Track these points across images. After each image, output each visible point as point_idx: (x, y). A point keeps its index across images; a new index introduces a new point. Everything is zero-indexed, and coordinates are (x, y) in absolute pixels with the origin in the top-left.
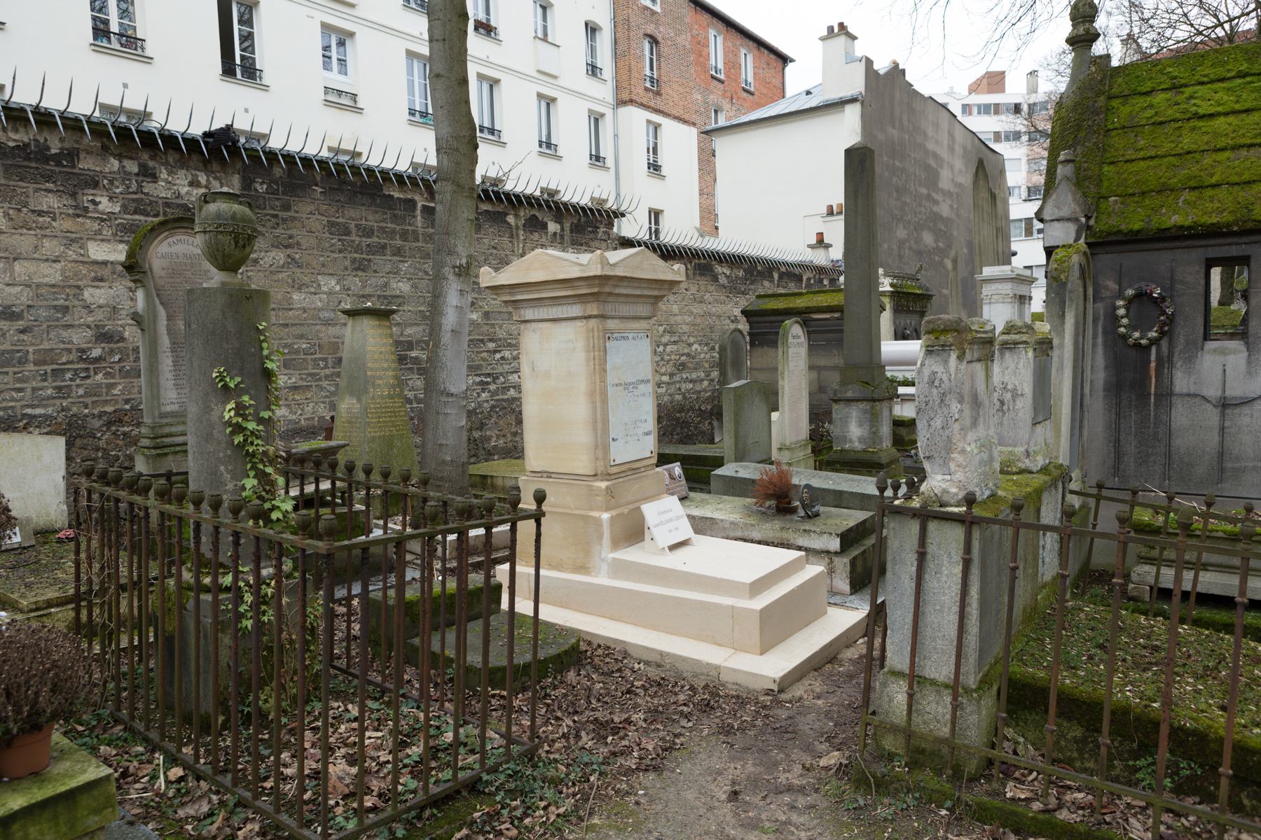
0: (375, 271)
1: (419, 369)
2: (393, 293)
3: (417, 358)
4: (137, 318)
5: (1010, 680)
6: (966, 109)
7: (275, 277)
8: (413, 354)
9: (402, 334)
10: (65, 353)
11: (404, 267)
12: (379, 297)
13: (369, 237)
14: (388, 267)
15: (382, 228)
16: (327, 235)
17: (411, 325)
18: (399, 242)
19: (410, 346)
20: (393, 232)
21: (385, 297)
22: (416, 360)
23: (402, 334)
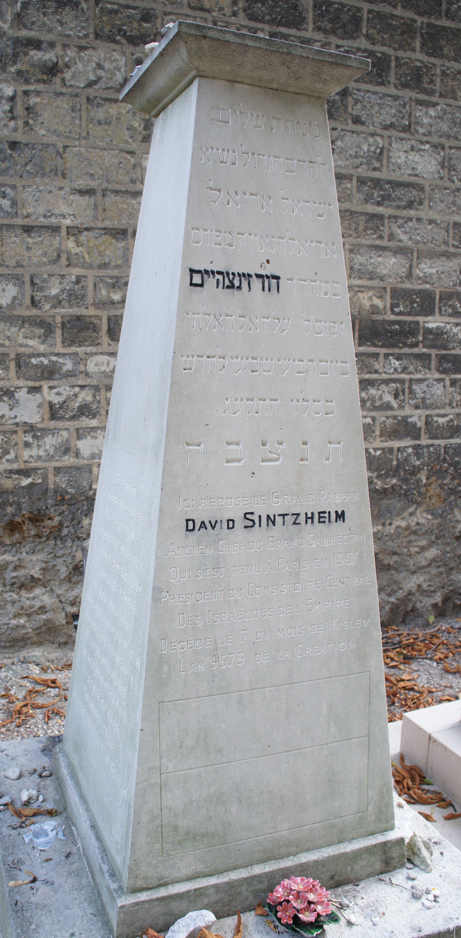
0: (357, 120)
1: (442, 359)
2: (396, 176)
3: (438, 333)
4: (108, 130)
5: (77, 597)
6: (353, 89)
7: (100, 114)
8: (433, 323)
9: (410, 275)
10: (83, 376)
11: (426, 117)
12: (362, 181)
13: (349, 35)
14: (388, 114)
15: (380, 16)
16: (242, 19)
17: (433, 255)
18: (418, 56)
19: (427, 303)
20: (408, 29)
21: (377, 183)
22: (437, 338)
23: (410, 275)
